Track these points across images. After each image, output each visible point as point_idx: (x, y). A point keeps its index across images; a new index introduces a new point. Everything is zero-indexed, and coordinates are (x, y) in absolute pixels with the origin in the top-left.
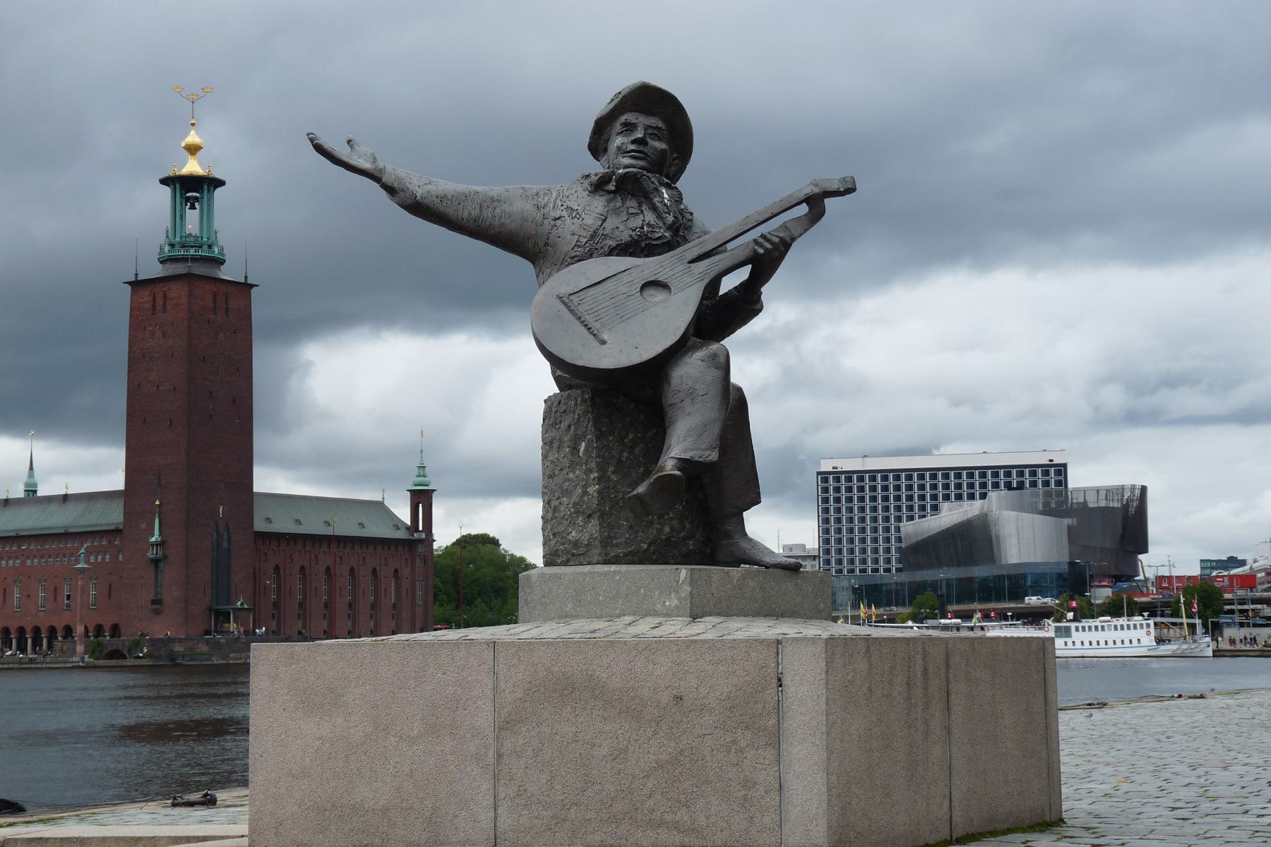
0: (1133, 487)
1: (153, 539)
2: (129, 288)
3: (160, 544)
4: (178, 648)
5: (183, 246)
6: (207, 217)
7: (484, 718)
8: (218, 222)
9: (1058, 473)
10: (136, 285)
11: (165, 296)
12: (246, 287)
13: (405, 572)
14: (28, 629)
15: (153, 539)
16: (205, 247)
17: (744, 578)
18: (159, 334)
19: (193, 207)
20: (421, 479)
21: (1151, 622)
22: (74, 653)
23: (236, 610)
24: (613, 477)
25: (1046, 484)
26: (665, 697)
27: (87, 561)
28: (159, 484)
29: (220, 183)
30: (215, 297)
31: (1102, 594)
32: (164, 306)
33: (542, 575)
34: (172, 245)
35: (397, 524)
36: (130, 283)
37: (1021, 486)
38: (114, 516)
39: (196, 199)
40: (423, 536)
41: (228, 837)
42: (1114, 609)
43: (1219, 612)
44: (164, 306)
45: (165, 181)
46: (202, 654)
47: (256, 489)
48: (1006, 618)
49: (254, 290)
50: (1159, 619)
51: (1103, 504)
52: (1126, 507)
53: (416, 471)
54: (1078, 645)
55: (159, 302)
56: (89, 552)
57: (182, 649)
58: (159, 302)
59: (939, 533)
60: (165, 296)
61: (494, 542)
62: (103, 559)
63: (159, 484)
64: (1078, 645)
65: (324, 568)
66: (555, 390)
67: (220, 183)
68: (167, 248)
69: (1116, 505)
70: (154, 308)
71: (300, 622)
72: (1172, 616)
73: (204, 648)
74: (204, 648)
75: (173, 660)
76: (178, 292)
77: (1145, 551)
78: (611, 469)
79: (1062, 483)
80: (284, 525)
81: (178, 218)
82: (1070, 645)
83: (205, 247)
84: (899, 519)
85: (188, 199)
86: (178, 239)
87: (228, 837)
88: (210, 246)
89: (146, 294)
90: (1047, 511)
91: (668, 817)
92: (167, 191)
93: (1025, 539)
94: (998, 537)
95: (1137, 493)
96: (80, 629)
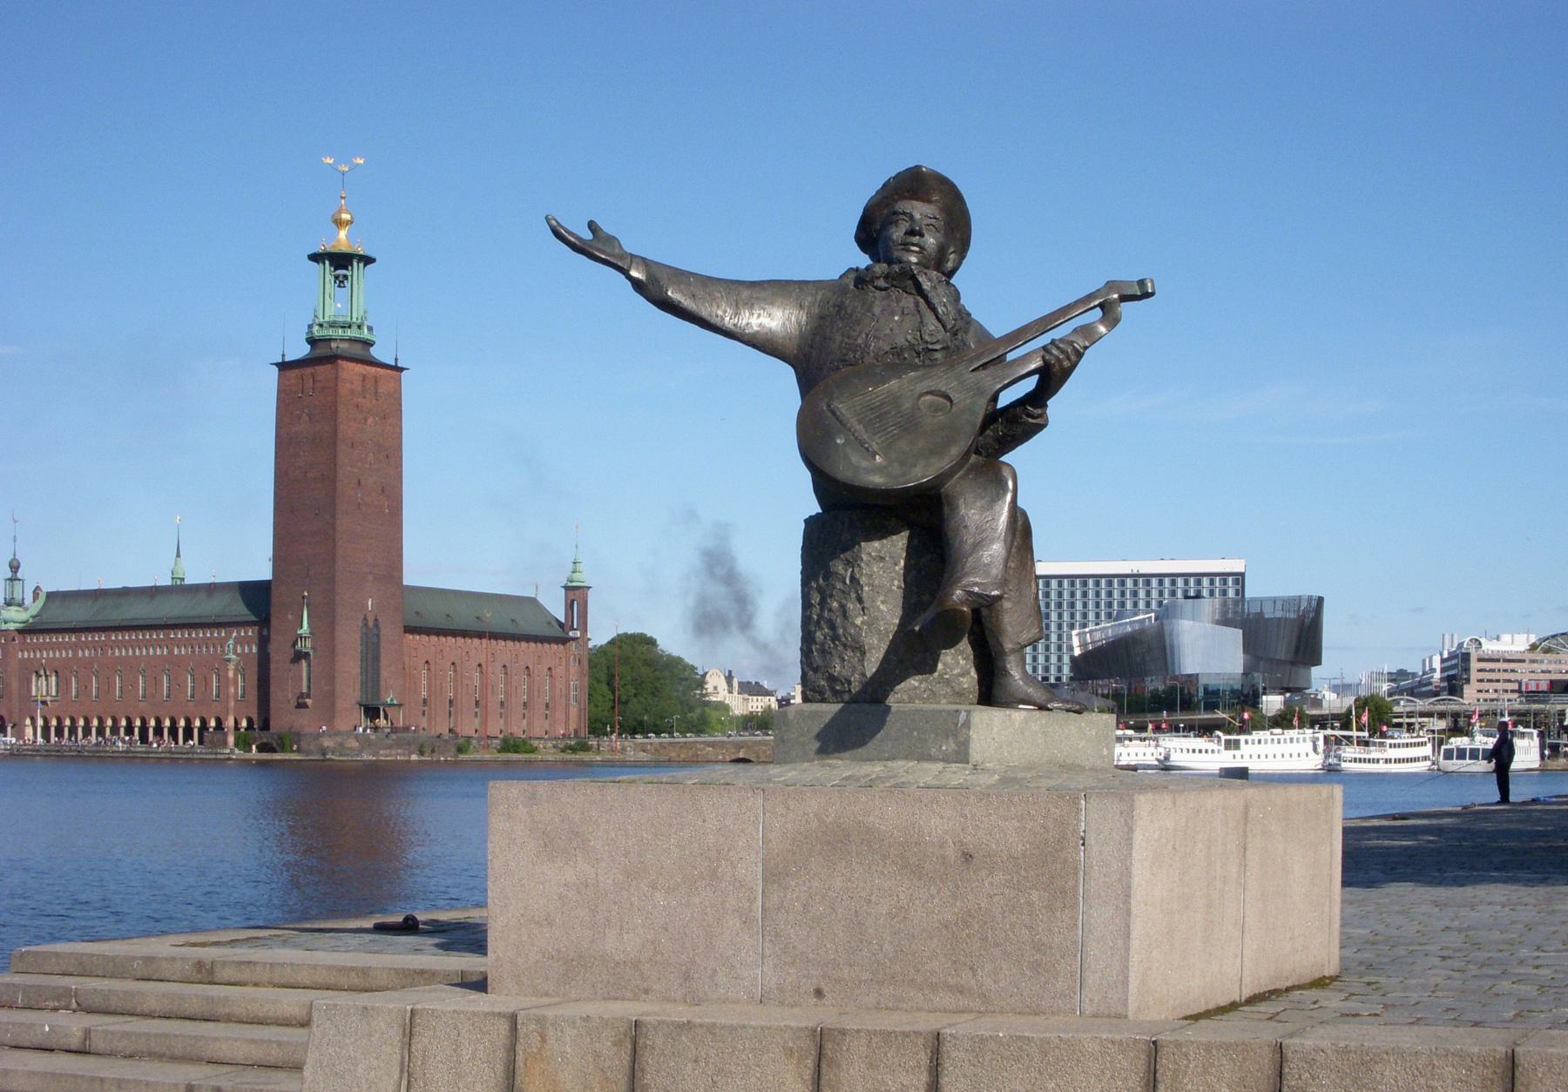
0: (1310, 598)
2: (276, 369)
7: (751, 870)
9: (1236, 582)
10: (283, 366)
13: (559, 671)
16: (355, 327)
17: (1026, 721)
18: (305, 417)
21: (1321, 735)
22: (225, 744)
24: (882, 607)
25: (1224, 593)
26: (951, 853)
27: (235, 652)
31: (1273, 703)
33: (800, 712)
37: (1198, 596)
40: (578, 634)
42: (1282, 721)
43: (1382, 722)
45: (316, 258)
47: (406, 582)
48: (1177, 730)
50: (1329, 732)
51: (1279, 614)
52: (1301, 619)
54: (1246, 757)
56: (238, 641)
61: (651, 642)
64: (1246, 757)
66: (815, 509)
69: (1292, 616)
72: (1341, 728)
73: (353, 744)
77: (1318, 662)
78: (881, 598)
79: (1240, 592)
82: (1238, 757)
83: (355, 327)
84: (1072, 627)
88: (359, 327)
89: (294, 373)
90: (1225, 621)
91: (951, 981)
93: (1208, 652)
94: (1172, 647)
95: (1314, 603)
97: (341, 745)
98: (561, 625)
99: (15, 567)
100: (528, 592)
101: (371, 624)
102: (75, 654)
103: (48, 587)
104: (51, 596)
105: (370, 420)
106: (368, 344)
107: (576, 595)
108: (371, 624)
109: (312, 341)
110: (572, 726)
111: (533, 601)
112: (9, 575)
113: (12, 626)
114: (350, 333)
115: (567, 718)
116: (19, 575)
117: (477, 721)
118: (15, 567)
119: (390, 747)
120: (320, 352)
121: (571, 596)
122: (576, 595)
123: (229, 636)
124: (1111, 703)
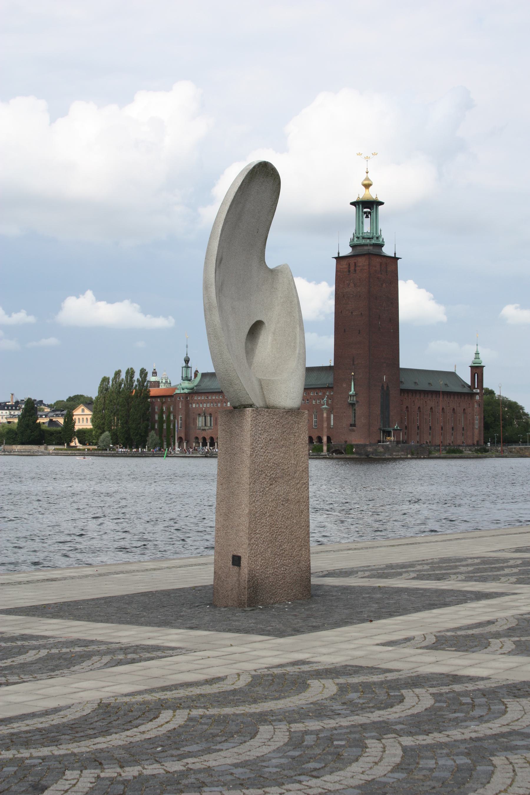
1: (351, 393)
2: (335, 260)
3: (356, 395)
4: (369, 449)
5: (363, 238)
6: (375, 224)
8: (381, 225)
10: (339, 259)
11: (355, 265)
12: (395, 259)
14: (208, 438)
15: (351, 393)
16: (375, 239)
18: (352, 285)
19: (367, 217)
20: (477, 360)
23: (394, 430)
27: (327, 404)
28: (353, 364)
29: (382, 203)
30: (381, 265)
32: (355, 271)
34: (358, 238)
35: (464, 384)
36: (335, 258)
38: (328, 379)
39: (370, 213)
40: (478, 391)
41: (388, 546)
44: (355, 271)
46: (381, 452)
49: (399, 261)
53: (474, 356)
55: (352, 268)
57: (371, 450)
58: (352, 268)
59: (95, 296)
60: (355, 265)
62: (316, 402)
63: (353, 364)
65: (429, 408)
67: (382, 203)
68: (355, 239)
70: (349, 271)
71: (418, 436)
74: (381, 450)
75: (368, 456)
76: (362, 262)
80: (409, 385)
81: (359, 223)
83: (375, 239)
85: (365, 213)
86: (361, 234)
87: (388, 546)
88: (377, 238)
92: (353, 208)
96: (325, 439)
97: (376, 450)
98: (469, 387)
99: (187, 361)
100: (452, 370)
101: (385, 389)
102: (222, 405)
103: (201, 371)
104: (204, 375)
105: (384, 285)
106: (382, 246)
107: (477, 370)
108: (385, 389)
109: (353, 246)
110: (476, 439)
111: (453, 374)
112: (184, 364)
113: (186, 391)
114: (373, 241)
115: (473, 435)
116: (189, 365)
117: (430, 437)
118: (187, 361)
119: (398, 451)
120: (359, 250)
121: (474, 371)
122: (477, 370)
123: (324, 394)
124: (313, 592)
